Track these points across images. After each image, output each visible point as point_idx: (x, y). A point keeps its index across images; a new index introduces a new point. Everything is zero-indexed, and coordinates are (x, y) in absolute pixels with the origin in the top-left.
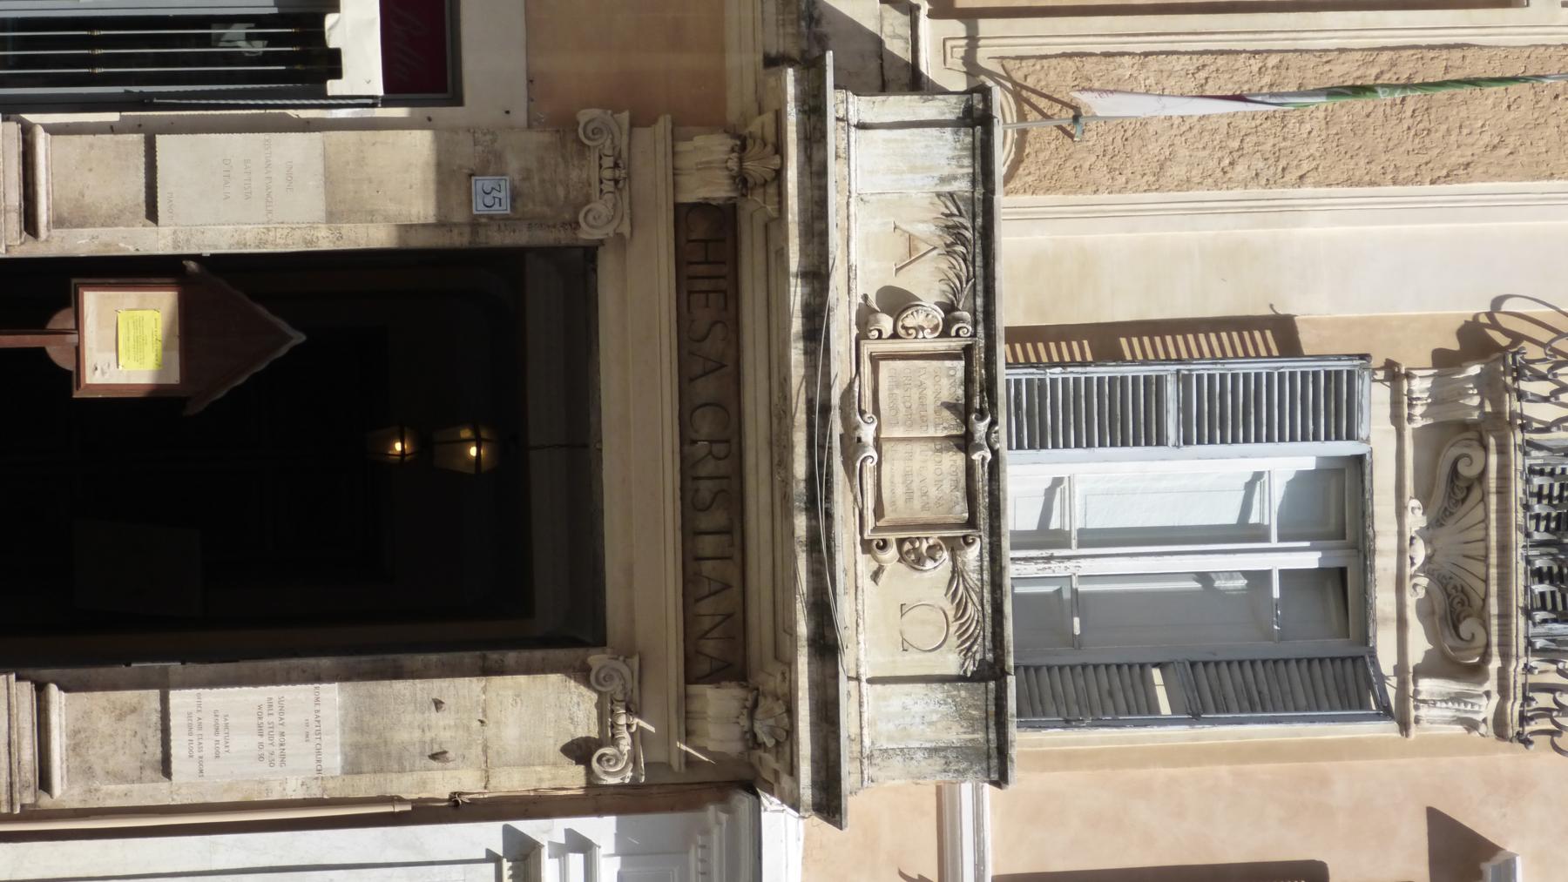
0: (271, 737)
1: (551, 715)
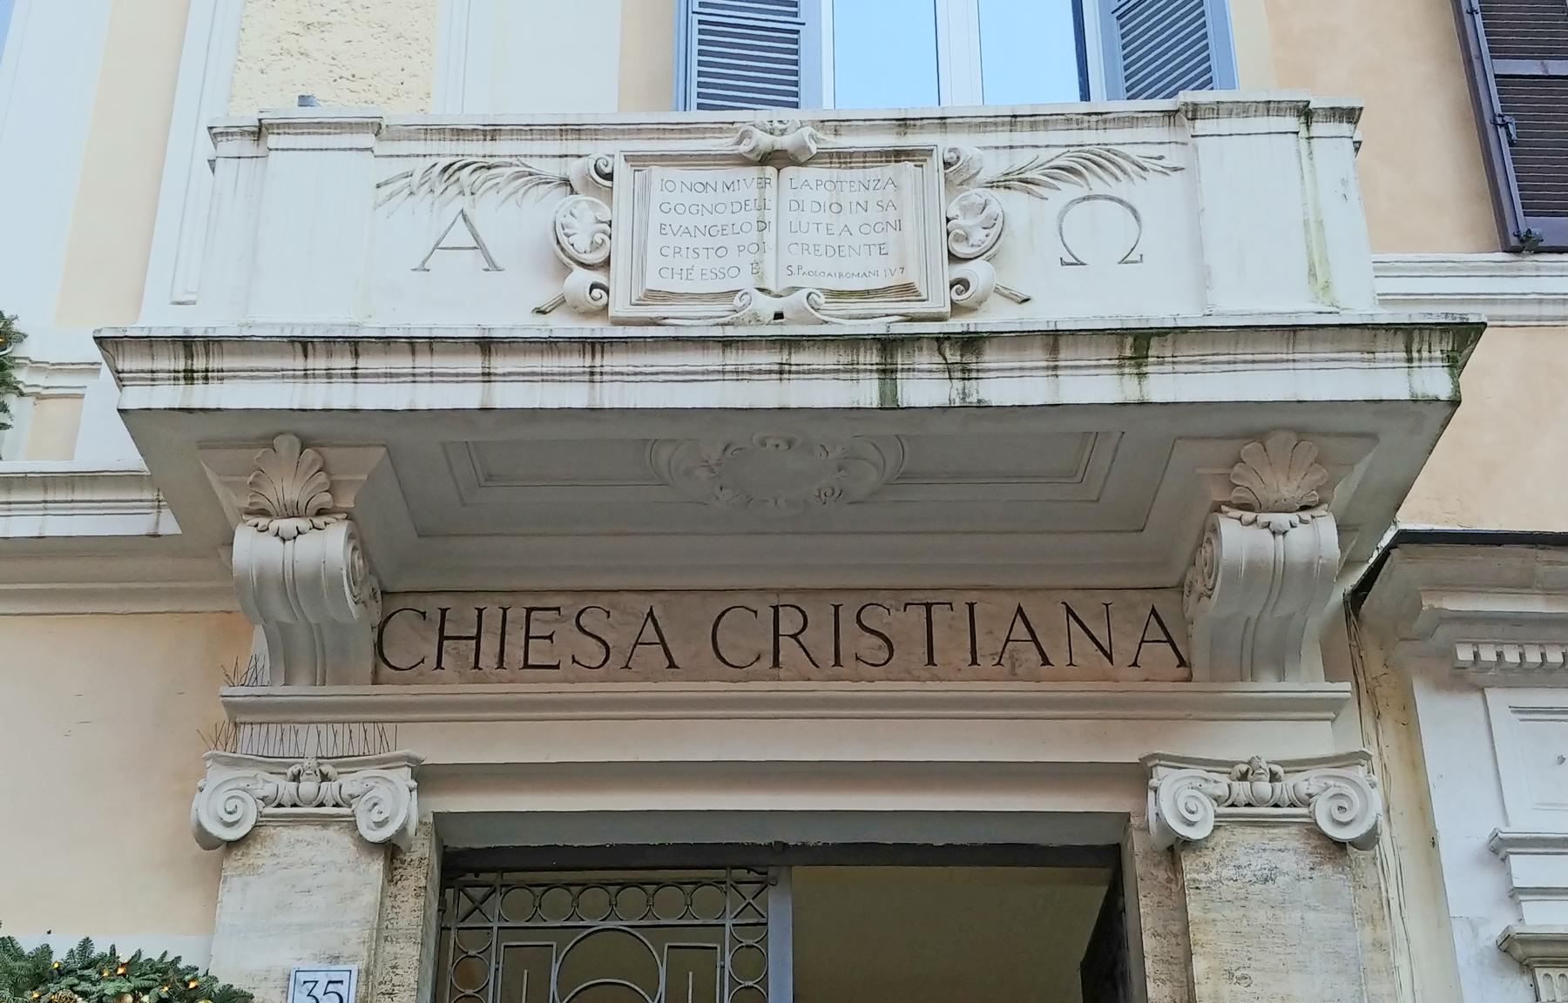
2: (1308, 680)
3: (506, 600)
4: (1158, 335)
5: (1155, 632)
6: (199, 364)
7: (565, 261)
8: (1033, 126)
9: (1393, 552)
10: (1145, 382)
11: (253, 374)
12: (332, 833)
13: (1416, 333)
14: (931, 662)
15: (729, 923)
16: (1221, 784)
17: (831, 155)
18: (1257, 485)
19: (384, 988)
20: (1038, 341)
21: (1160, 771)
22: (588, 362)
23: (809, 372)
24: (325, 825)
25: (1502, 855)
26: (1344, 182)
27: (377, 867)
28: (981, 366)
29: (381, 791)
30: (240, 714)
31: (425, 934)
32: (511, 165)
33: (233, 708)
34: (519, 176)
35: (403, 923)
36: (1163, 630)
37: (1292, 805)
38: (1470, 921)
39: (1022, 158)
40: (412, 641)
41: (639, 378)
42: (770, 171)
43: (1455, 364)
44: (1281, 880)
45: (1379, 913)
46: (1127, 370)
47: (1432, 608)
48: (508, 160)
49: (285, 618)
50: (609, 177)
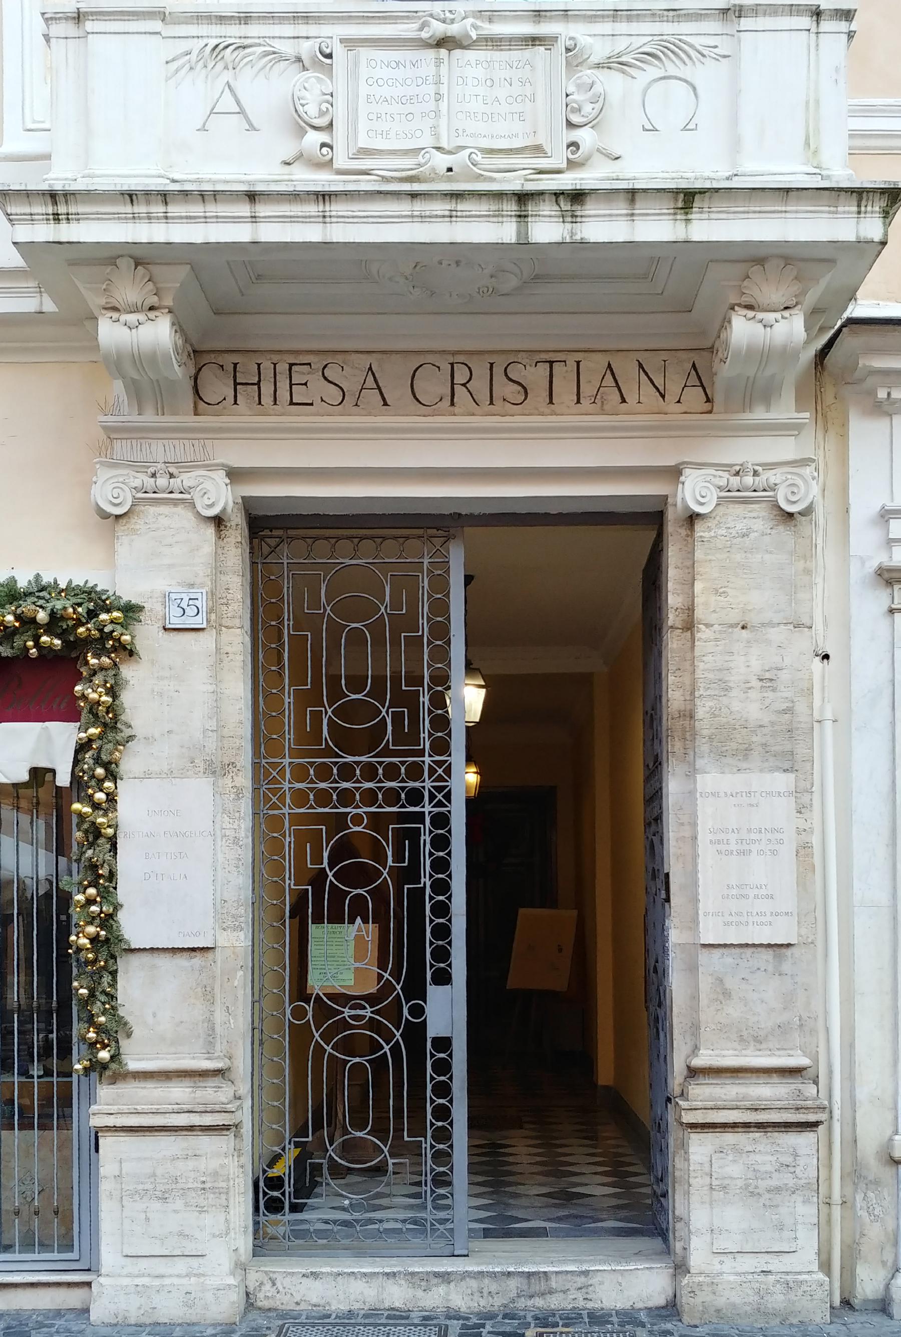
0: (754, 841)
1: (738, 557)
2: (785, 410)
3: (275, 358)
4: (700, 193)
5: (693, 379)
6: (62, 209)
7: (301, 126)
8: (629, 19)
9: (844, 329)
10: (689, 226)
11: (100, 217)
12: (180, 510)
13: (865, 194)
14: (551, 402)
15: (426, 561)
16: (724, 478)
17: (486, 40)
18: (756, 292)
19: (222, 601)
20: (622, 196)
21: (687, 472)
22: (321, 208)
23: (469, 216)
24: (175, 505)
25: (886, 518)
26: (837, 69)
27: (210, 531)
28: (583, 213)
29: (208, 485)
30: (113, 433)
31: (244, 569)
32: (260, 45)
33: (107, 429)
34: (267, 54)
35: (230, 564)
36: (700, 380)
37: (765, 490)
38: (861, 558)
39: (621, 44)
40: (217, 387)
41: (355, 220)
42: (443, 52)
43: (887, 215)
44: (753, 535)
45: (809, 552)
46: (679, 217)
47: (864, 365)
48: (257, 41)
49: (136, 377)
50: (329, 56)
